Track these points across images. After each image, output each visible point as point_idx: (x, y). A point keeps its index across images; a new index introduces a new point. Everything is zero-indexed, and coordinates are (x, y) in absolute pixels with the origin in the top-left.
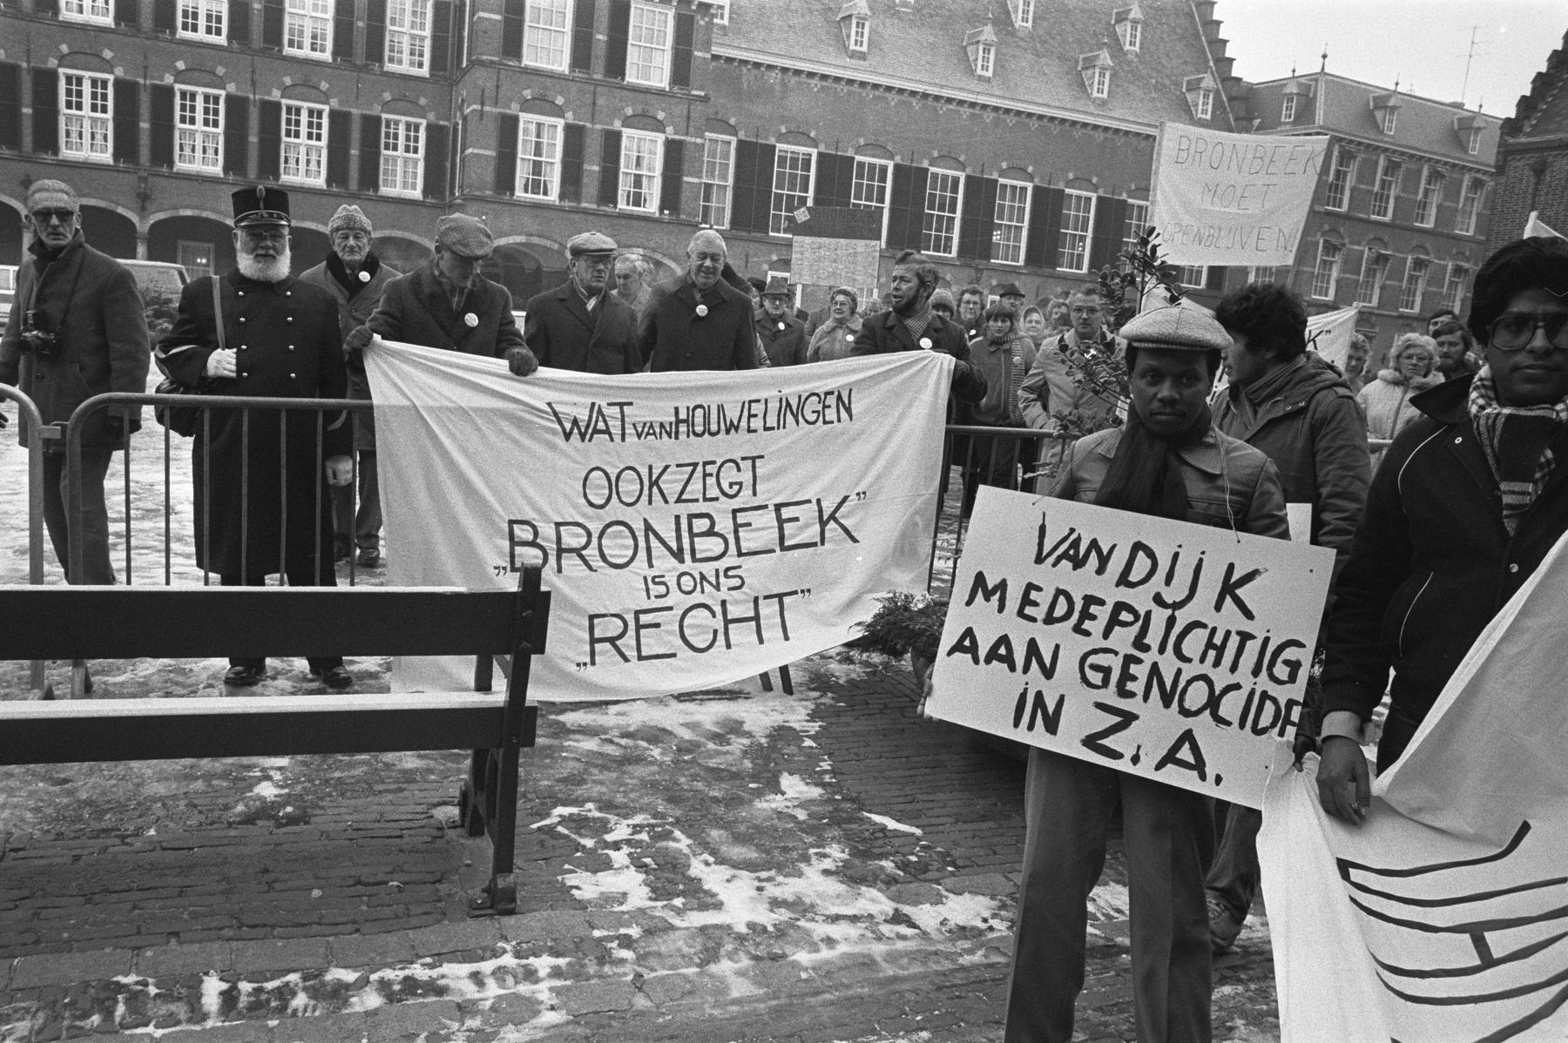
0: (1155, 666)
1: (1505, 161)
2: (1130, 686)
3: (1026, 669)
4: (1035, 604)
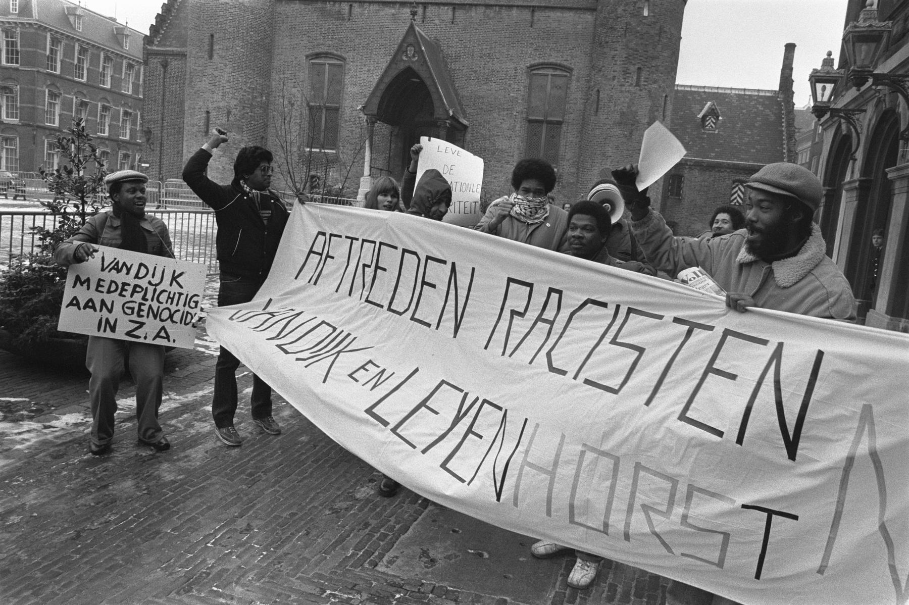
0: (150, 306)
1: (148, 59)
2: (142, 313)
3: (101, 310)
4: (102, 286)
